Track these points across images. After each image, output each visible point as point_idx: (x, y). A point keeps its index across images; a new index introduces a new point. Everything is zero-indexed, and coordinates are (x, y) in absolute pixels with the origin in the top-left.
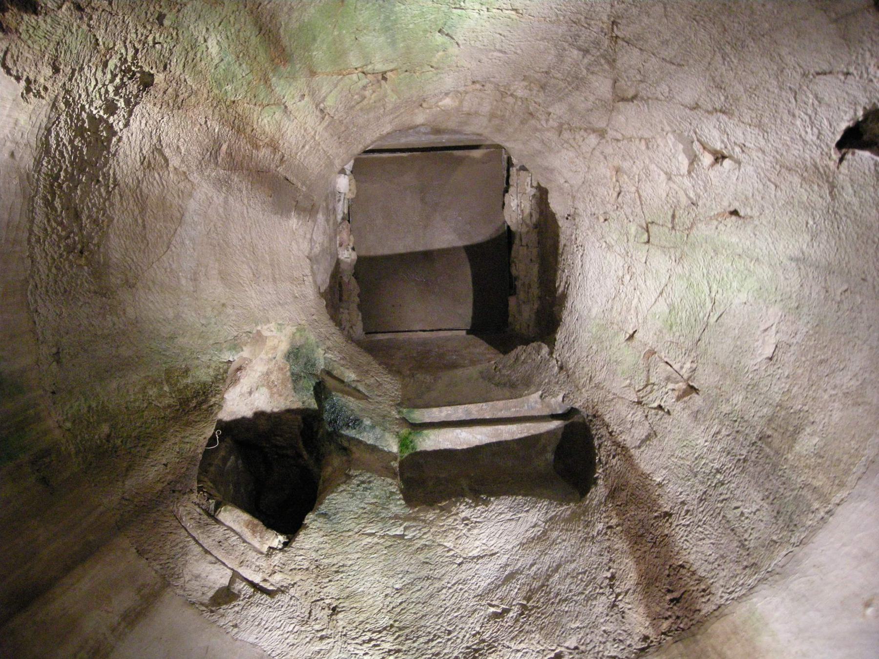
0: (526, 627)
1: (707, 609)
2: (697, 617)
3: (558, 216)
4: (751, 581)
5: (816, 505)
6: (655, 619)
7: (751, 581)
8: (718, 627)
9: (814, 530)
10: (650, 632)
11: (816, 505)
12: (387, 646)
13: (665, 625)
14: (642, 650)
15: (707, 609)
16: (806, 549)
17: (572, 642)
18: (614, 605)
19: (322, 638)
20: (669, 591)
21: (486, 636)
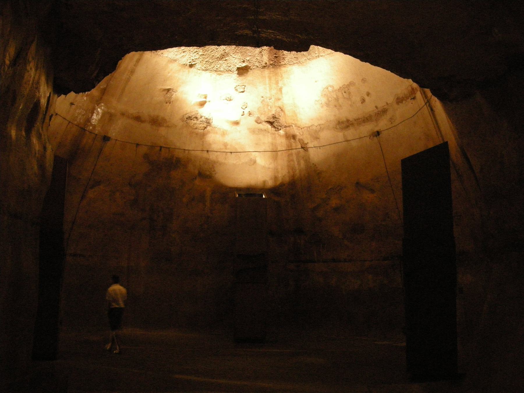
0: (237, 51)
1: (282, 63)
2: (280, 64)
3: (278, 51)
4: (295, 62)
5: (316, 52)
6: (270, 60)
7: (295, 62)
8: (283, 69)
9: (313, 58)
10: (267, 62)
11: (316, 52)
12: (200, 53)
13: (272, 62)
14: (265, 66)
15: (282, 63)
16: (310, 62)
17: (248, 59)
18: (261, 52)
19: (184, 52)
20: (275, 54)
21: (226, 51)
